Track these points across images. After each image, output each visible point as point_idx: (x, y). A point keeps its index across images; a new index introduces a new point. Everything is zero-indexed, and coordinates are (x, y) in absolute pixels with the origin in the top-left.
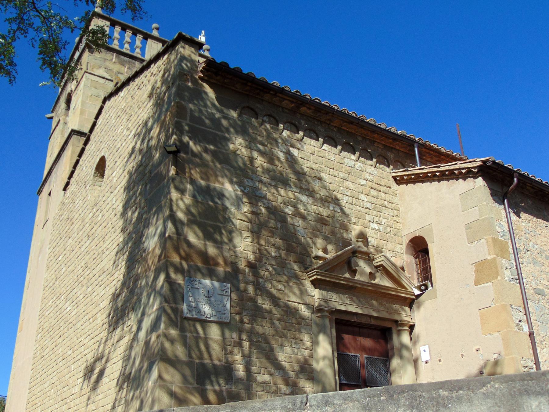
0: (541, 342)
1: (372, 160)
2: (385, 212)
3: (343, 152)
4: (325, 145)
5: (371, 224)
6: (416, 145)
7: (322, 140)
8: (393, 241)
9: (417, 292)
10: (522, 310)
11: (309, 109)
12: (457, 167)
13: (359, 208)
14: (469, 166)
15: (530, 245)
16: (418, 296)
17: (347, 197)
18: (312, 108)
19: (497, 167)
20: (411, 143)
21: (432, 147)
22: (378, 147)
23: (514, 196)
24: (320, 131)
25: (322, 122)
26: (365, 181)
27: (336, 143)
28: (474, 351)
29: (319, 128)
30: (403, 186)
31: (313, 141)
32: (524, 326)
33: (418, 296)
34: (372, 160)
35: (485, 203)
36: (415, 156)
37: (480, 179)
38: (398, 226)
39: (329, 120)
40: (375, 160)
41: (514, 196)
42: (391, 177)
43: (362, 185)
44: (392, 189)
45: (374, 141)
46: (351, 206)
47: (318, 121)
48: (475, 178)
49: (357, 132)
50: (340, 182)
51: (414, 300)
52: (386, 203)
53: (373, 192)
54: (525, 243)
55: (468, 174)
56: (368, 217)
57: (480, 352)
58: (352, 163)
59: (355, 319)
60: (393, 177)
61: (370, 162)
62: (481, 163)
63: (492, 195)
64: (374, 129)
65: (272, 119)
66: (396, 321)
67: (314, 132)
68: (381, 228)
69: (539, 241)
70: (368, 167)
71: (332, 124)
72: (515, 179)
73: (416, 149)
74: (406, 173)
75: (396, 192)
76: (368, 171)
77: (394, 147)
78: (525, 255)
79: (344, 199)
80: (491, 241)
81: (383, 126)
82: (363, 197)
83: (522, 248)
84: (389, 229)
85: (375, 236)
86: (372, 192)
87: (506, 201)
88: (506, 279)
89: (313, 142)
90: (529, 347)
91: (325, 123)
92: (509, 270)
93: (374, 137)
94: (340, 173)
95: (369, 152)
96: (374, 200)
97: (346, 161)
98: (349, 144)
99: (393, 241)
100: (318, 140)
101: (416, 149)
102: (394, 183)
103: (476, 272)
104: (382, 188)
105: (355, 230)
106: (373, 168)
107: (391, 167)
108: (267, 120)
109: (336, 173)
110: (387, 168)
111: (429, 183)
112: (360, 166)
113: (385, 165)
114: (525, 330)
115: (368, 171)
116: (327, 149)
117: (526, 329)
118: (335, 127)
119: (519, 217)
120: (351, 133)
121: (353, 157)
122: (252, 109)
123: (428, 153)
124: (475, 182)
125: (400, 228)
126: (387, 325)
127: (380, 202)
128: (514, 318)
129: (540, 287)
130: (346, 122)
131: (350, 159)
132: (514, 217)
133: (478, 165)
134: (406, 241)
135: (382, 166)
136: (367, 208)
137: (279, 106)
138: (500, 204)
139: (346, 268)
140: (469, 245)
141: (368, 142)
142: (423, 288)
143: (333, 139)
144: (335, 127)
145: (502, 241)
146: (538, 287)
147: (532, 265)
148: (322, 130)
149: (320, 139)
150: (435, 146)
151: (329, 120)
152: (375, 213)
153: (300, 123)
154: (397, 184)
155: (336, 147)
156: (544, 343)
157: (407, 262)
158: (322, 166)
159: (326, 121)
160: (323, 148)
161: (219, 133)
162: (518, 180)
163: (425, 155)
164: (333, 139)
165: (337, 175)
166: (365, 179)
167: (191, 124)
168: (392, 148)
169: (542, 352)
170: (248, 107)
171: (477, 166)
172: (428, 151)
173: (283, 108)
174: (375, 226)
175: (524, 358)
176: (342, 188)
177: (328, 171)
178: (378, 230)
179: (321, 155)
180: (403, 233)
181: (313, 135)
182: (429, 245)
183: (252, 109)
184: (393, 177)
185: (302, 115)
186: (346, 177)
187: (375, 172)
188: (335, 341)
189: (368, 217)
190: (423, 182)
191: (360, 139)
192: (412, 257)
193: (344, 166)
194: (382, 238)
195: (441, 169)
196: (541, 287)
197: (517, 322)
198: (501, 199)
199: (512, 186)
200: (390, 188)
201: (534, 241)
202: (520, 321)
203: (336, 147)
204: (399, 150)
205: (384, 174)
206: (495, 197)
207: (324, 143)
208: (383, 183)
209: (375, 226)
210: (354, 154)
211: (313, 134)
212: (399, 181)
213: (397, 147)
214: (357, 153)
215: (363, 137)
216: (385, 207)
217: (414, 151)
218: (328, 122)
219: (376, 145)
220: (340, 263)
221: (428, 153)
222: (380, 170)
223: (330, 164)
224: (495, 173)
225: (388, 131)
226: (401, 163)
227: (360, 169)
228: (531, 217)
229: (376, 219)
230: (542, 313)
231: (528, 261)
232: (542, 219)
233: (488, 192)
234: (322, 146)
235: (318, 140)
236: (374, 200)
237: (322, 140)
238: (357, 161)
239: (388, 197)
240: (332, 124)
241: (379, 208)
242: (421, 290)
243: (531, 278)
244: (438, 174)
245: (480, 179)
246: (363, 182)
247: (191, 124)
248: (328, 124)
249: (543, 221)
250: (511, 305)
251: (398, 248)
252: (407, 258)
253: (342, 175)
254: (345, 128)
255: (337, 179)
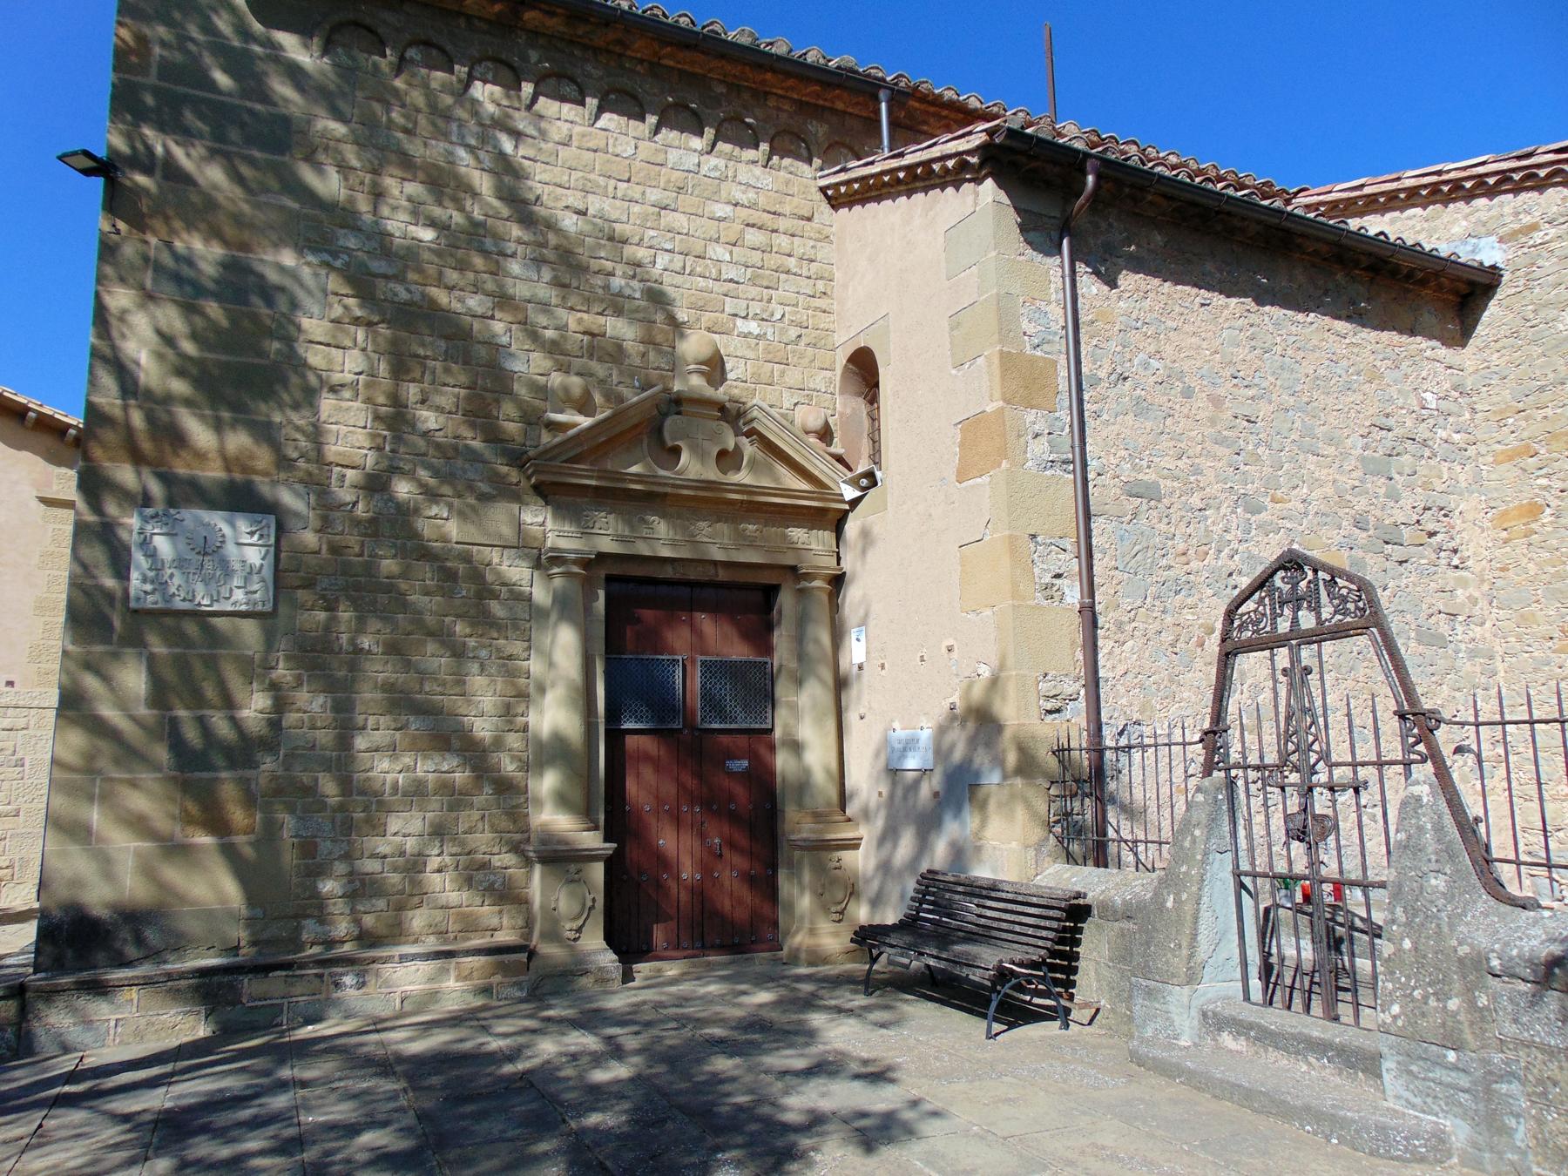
0: (1120, 626)
1: (756, 147)
2: (787, 289)
3: (664, 130)
4: (606, 116)
5: (739, 322)
6: (882, 95)
7: (595, 102)
8: (805, 361)
9: (850, 493)
10: (1069, 547)
11: (552, 14)
12: (936, 152)
13: (702, 282)
14: (961, 149)
15: (1136, 361)
16: (854, 503)
17: (667, 256)
18: (559, 11)
19: (1025, 147)
20: (864, 88)
21: (940, 96)
22: (779, 109)
23: (1104, 225)
24: (590, 76)
25: (596, 51)
26: (729, 208)
27: (641, 106)
28: (944, 650)
29: (589, 68)
30: (844, 211)
31: (566, 107)
32: (1067, 591)
33: (854, 503)
34: (756, 147)
35: (994, 254)
36: (879, 121)
37: (989, 182)
38: (824, 321)
39: (620, 42)
40: (764, 147)
41: (1104, 225)
42: (814, 190)
43: (719, 220)
44: (815, 224)
45: (767, 93)
46: (679, 279)
47: (585, 47)
48: (978, 181)
49: (710, 70)
50: (646, 218)
51: (845, 514)
52: (792, 263)
53: (753, 237)
54: (1117, 358)
55: (957, 174)
56: (730, 305)
57: (955, 655)
58: (691, 161)
59: (668, 573)
60: (823, 190)
61: (750, 154)
62: (984, 137)
63: (1023, 228)
64: (754, 59)
65: (434, 52)
66: (794, 569)
67: (572, 80)
68: (770, 332)
69: (1168, 350)
70: (742, 168)
71: (629, 53)
72: (1090, 178)
73: (883, 106)
74: (843, 177)
75: (827, 231)
76: (742, 178)
77: (828, 104)
78: (1112, 393)
79: (659, 260)
80: (996, 361)
81: (780, 49)
82: (720, 252)
83: (1102, 374)
84: (793, 332)
85: (751, 354)
86: (747, 237)
87: (1065, 242)
88: (1030, 464)
89: (567, 109)
90: (1073, 643)
91: (608, 52)
92: (1044, 440)
93: (763, 82)
94: (648, 190)
95: (749, 126)
96: (756, 257)
97: (673, 156)
98: (687, 107)
99: (805, 361)
100: (583, 104)
101: (883, 106)
102: (825, 207)
103: (962, 445)
104: (782, 224)
105: (693, 346)
106: (758, 170)
107: (817, 162)
108: (418, 58)
109: (635, 192)
110: (806, 167)
111: (890, 202)
112: (716, 168)
113: (798, 157)
114: (1068, 600)
115: (740, 178)
116: (612, 126)
117: (1073, 594)
118: (641, 61)
119: (1113, 284)
120: (693, 75)
121: (697, 143)
122: (370, 30)
123: (934, 115)
124: (977, 194)
125: (832, 327)
126: (766, 578)
127: (773, 260)
128: (1036, 570)
129: (1146, 478)
130: (671, 44)
131: (686, 150)
132: (1089, 286)
133: (977, 143)
134: (841, 358)
135: (787, 161)
136: (731, 281)
137: (459, 14)
138: (1048, 254)
139: (645, 446)
140: (954, 372)
141: (746, 96)
142: (864, 482)
143: (634, 97)
144: (641, 61)
145: (1033, 361)
146: (1140, 477)
147: (1130, 418)
148: (597, 73)
149: (588, 100)
150: (949, 95)
151: (620, 42)
152: (754, 291)
153: (525, 59)
154: (833, 207)
155: (643, 120)
156: (1129, 628)
157: (841, 415)
158: (592, 176)
159: (611, 47)
160: (600, 124)
161: (259, 107)
162: (1099, 178)
163: (925, 122)
164: (634, 97)
165: (637, 196)
166: (729, 203)
167: (163, 84)
168: (823, 108)
169: (1117, 651)
170: (357, 24)
171: (978, 148)
172: (932, 109)
173: (469, 18)
174: (753, 327)
175: (1052, 673)
176: (652, 233)
177: (611, 189)
178: (758, 337)
179: (591, 145)
180: (839, 338)
181: (569, 89)
182: (881, 371)
183: (370, 30)
184: (823, 190)
185: (534, 34)
186: (666, 202)
187: (764, 178)
188: (600, 631)
189: (730, 305)
190: (878, 199)
191: (721, 89)
192: (861, 400)
193: (664, 170)
194: (770, 357)
195: (909, 160)
196: (1149, 476)
197: (1047, 579)
198: (1055, 235)
199: (1082, 200)
200: (809, 219)
201: (1152, 349)
202: (1058, 576)
203: (643, 120)
204: (845, 112)
205: (802, 180)
206: (1032, 235)
207: (601, 110)
208: (787, 209)
209: (753, 327)
210: (701, 134)
211: (565, 83)
212: (837, 199)
213: (840, 106)
214: (709, 133)
215: (730, 86)
216: (788, 272)
217: (878, 112)
218: (618, 49)
219: (772, 102)
220: (622, 433)
221: (934, 115)
222: (782, 173)
223: (619, 169)
224: (1034, 164)
225: (801, 64)
226: (851, 149)
227: (717, 174)
228: (1157, 281)
229: (756, 308)
230: (1137, 548)
231: (1119, 409)
232: (1195, 285)
233: (1012, 218)
234: (597, 118)
235: (583, 104)
236: (756, 257)
237: (595, 102)
238: (709, 153)
239: (800, 247)
240: (629, 53)
241: (765, 279)
242: (864, 489)
243: (1123, 453)
244: (901, 175)
245: (989, 182)
246: (721, 210)
247: (163, 84)
248: (620, 55)
249: (1195, 290)
250: (1034, 536)
251: (819, 380)
252: (845, 405)
253: (654, 195)
254: (671, 63)
255: (636, 209)
